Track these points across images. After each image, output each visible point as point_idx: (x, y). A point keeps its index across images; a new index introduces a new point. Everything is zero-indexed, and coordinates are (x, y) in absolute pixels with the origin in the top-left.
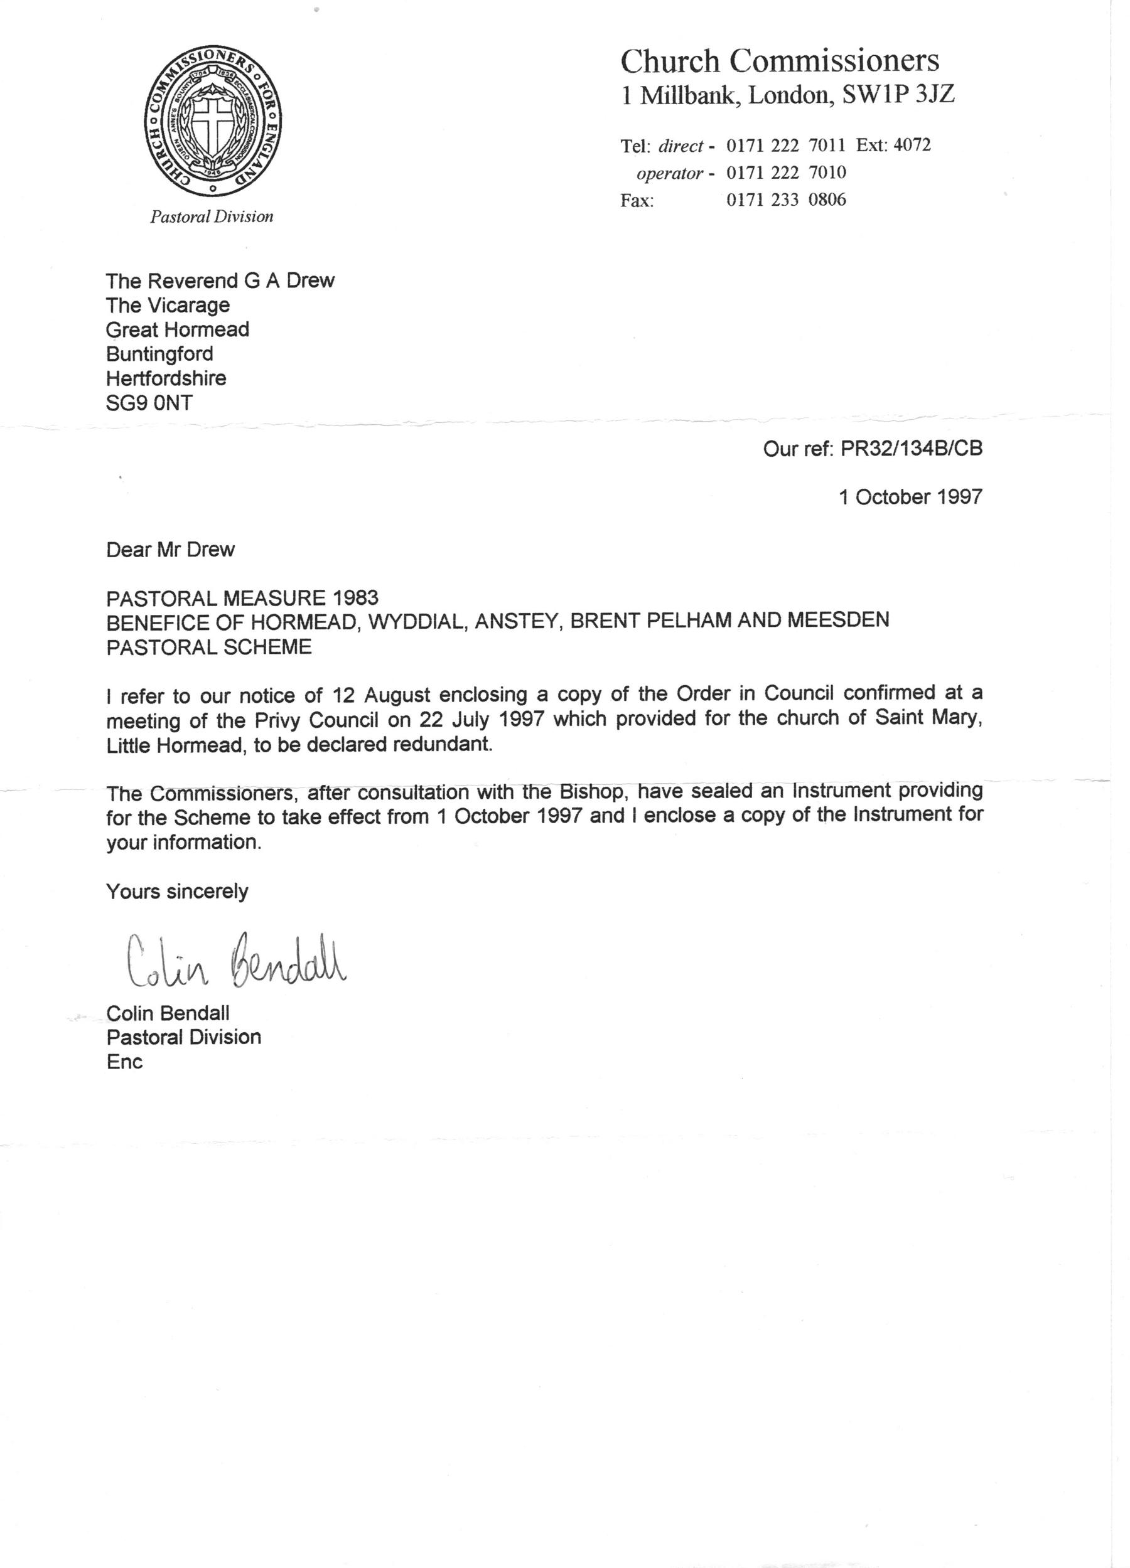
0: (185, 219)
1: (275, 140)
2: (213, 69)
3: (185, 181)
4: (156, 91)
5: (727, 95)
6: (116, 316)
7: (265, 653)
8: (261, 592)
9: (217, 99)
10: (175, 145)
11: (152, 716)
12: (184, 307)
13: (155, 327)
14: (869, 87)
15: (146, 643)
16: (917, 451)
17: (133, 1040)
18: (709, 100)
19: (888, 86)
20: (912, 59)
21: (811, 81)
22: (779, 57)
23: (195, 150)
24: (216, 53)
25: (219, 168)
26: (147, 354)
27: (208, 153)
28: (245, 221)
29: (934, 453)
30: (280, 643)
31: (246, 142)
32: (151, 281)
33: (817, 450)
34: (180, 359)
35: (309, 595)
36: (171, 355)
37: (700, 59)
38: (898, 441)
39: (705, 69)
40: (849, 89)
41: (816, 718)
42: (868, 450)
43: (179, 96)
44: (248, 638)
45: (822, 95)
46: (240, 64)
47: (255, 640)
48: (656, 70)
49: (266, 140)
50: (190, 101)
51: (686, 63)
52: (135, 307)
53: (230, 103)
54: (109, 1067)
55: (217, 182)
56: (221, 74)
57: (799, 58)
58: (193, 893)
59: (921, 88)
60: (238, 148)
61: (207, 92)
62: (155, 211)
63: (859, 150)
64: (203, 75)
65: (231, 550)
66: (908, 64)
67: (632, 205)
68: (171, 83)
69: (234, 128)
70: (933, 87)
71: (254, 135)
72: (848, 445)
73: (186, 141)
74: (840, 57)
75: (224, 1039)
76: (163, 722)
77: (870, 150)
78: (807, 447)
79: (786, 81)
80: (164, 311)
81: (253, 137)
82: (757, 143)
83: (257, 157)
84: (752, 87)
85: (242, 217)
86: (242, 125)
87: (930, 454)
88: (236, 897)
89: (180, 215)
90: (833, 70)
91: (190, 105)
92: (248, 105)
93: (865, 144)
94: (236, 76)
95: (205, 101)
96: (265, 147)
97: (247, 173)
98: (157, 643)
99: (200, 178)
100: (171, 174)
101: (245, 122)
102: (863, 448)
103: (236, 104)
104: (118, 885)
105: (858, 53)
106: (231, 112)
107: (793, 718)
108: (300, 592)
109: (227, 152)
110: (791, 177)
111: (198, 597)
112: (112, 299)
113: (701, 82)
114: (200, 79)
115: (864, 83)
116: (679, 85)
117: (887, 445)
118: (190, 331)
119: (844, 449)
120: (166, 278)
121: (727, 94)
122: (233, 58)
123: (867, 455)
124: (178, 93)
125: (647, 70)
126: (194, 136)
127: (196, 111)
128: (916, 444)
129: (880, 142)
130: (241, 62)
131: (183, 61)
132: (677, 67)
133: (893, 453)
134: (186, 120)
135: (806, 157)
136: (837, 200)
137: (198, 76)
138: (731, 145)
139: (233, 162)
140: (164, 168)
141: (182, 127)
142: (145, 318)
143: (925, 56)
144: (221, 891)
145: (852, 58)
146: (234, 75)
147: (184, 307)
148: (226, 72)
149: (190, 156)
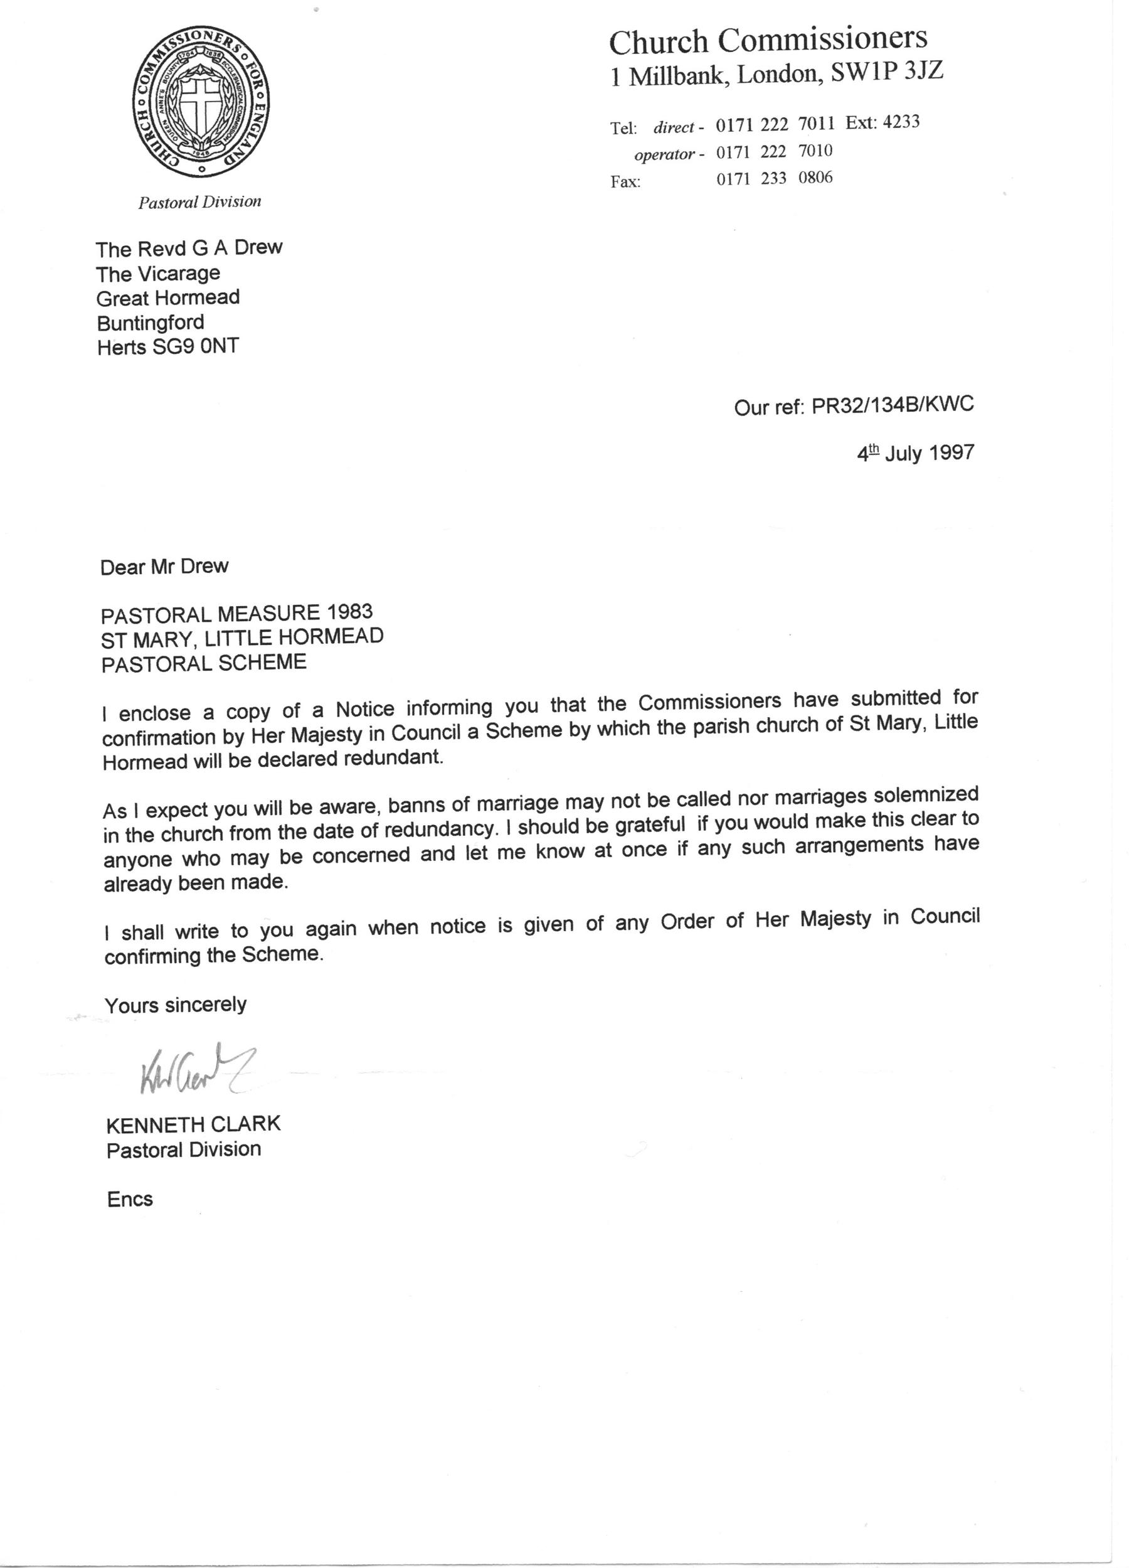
0: (173, 205)
1: (263, 119)
2: (200, 50)
3: (174, 162)
4: (143, 73)
5: (716, 75)
6: (107, 286)
7: (260, 668)
8: (255, 608)
9: (205, 80)
10: (164, 126)
11: (140, 318)
12: (175, 275)
13: (146, 295)
14: (857, 64)
15: (140, 611)
16: (888, 408)
17: (133, 1153)
18: (698, 80)
19: (876, 63)
20: (900, 35)
21: (800, 59)
22: (767, 36)
23: (183, 131)
24: (203, 34)
25: (208, 148)
26: (138, 324)
27: (196, 133)
28: (233, 206)
29: (905, 410)
30: (275, 658)
31: (234, 122)
32: (141, 249)
33: (788, 408)
34: (171, 328)
35: (303, 611)
36: (162, 324)
37: (689, 40)
38: (869, 398)
39: (693, 49)
40: (838, 67)
41: (796, 725)
42: (839, 407)
43: (167, 77)
44: (242, 654)
45: (811, 73)
46: (227, 44)
47: (250, 656)
48: (645, 52)
49: (255, 120)
50: (178, 82)
51: (675, 44)
52: (126, 276)
53: (218, 83)
54: (110, 1205)
55: (206, 163)
56: (208, 55)
57: (787, 37)
58: (191, 1006)
59: (910, 65)
60: (227, 128)
61: (194, 73)
62: (143, 198)
63: (849, 128)
64: (191, 55)
65: (224, 566)
66: (897, 41)
67: (622, 186)
68: (159, 64)
69: (222, 109)
70: (922, 63)
71: (242, 115)
72: (818, 403)
73: (174, 122)
74: (829, 35)
75: (224, 1151)
76: (150, 323)
77: (859, 128)
78: (778, 405)
79: (775, 60)
80: (154, 280)
81: (241, 117)
82: (746, 123)
83: (245, 137)
84: (741, 66)
85: (230, 202)
86: (230, 105)
87: (902, 411)
88: (234, 1010)
89: (168, 201)
90: (822, 48)
91: (178, 86)
92: (236, 85)
93: (854, 122)
94: (223, 57)
95: (193, 82)
96: (254, 127)
97: (236, 154)
98: (151, 611)
99: (189, 159)
100: (160, 155)
101: (233, 103)
102: (834, 406)
103: (224, 85)
104: (117, 999)
105: (846, 31)
106: (219, 92)
107: (772, 726)
108: (294, 606)
109: (215, 133)
110: (771, 129)
111: (193, 614)
112: (102, 269)
113: (689, 63)
114: (187, 61)
115: (853, 60)
116: (668, 66)
117: (858, 402)
118: (182, 299)
119: (815, 407)
120: (156, 247)
121: (716, 73)
122: (221, 38)
123: (838, 412)
124: (166, 74)
125: (636, 52)
126: (183, 117)
127: (183, 92)
128: (887, 401)
129: (869, 120)
130: (228, 42)
131: (170, 43)
132: (666, 48)
133: (864, 410)
134: (174, 101)
135: (795, 135)
136: (825, 177)
137: (186, 57)
138: (720, 125)
139: (222, 143)
140: (152, 149)
141: (170, 108)
142: (135, 286)
143: (913, 33)
144: (219, 1004)
145: (840, 35)
146: (221, 55)
147: (175, 275)
148: (213, 52)
149: (179, 138)
